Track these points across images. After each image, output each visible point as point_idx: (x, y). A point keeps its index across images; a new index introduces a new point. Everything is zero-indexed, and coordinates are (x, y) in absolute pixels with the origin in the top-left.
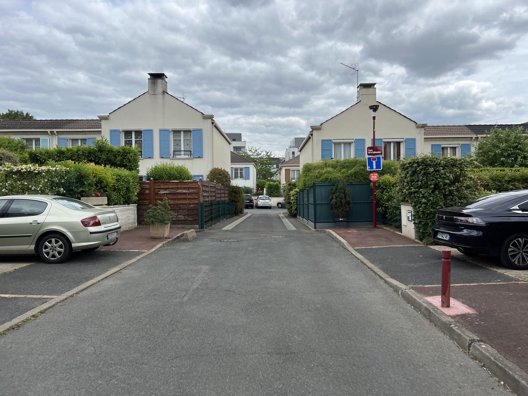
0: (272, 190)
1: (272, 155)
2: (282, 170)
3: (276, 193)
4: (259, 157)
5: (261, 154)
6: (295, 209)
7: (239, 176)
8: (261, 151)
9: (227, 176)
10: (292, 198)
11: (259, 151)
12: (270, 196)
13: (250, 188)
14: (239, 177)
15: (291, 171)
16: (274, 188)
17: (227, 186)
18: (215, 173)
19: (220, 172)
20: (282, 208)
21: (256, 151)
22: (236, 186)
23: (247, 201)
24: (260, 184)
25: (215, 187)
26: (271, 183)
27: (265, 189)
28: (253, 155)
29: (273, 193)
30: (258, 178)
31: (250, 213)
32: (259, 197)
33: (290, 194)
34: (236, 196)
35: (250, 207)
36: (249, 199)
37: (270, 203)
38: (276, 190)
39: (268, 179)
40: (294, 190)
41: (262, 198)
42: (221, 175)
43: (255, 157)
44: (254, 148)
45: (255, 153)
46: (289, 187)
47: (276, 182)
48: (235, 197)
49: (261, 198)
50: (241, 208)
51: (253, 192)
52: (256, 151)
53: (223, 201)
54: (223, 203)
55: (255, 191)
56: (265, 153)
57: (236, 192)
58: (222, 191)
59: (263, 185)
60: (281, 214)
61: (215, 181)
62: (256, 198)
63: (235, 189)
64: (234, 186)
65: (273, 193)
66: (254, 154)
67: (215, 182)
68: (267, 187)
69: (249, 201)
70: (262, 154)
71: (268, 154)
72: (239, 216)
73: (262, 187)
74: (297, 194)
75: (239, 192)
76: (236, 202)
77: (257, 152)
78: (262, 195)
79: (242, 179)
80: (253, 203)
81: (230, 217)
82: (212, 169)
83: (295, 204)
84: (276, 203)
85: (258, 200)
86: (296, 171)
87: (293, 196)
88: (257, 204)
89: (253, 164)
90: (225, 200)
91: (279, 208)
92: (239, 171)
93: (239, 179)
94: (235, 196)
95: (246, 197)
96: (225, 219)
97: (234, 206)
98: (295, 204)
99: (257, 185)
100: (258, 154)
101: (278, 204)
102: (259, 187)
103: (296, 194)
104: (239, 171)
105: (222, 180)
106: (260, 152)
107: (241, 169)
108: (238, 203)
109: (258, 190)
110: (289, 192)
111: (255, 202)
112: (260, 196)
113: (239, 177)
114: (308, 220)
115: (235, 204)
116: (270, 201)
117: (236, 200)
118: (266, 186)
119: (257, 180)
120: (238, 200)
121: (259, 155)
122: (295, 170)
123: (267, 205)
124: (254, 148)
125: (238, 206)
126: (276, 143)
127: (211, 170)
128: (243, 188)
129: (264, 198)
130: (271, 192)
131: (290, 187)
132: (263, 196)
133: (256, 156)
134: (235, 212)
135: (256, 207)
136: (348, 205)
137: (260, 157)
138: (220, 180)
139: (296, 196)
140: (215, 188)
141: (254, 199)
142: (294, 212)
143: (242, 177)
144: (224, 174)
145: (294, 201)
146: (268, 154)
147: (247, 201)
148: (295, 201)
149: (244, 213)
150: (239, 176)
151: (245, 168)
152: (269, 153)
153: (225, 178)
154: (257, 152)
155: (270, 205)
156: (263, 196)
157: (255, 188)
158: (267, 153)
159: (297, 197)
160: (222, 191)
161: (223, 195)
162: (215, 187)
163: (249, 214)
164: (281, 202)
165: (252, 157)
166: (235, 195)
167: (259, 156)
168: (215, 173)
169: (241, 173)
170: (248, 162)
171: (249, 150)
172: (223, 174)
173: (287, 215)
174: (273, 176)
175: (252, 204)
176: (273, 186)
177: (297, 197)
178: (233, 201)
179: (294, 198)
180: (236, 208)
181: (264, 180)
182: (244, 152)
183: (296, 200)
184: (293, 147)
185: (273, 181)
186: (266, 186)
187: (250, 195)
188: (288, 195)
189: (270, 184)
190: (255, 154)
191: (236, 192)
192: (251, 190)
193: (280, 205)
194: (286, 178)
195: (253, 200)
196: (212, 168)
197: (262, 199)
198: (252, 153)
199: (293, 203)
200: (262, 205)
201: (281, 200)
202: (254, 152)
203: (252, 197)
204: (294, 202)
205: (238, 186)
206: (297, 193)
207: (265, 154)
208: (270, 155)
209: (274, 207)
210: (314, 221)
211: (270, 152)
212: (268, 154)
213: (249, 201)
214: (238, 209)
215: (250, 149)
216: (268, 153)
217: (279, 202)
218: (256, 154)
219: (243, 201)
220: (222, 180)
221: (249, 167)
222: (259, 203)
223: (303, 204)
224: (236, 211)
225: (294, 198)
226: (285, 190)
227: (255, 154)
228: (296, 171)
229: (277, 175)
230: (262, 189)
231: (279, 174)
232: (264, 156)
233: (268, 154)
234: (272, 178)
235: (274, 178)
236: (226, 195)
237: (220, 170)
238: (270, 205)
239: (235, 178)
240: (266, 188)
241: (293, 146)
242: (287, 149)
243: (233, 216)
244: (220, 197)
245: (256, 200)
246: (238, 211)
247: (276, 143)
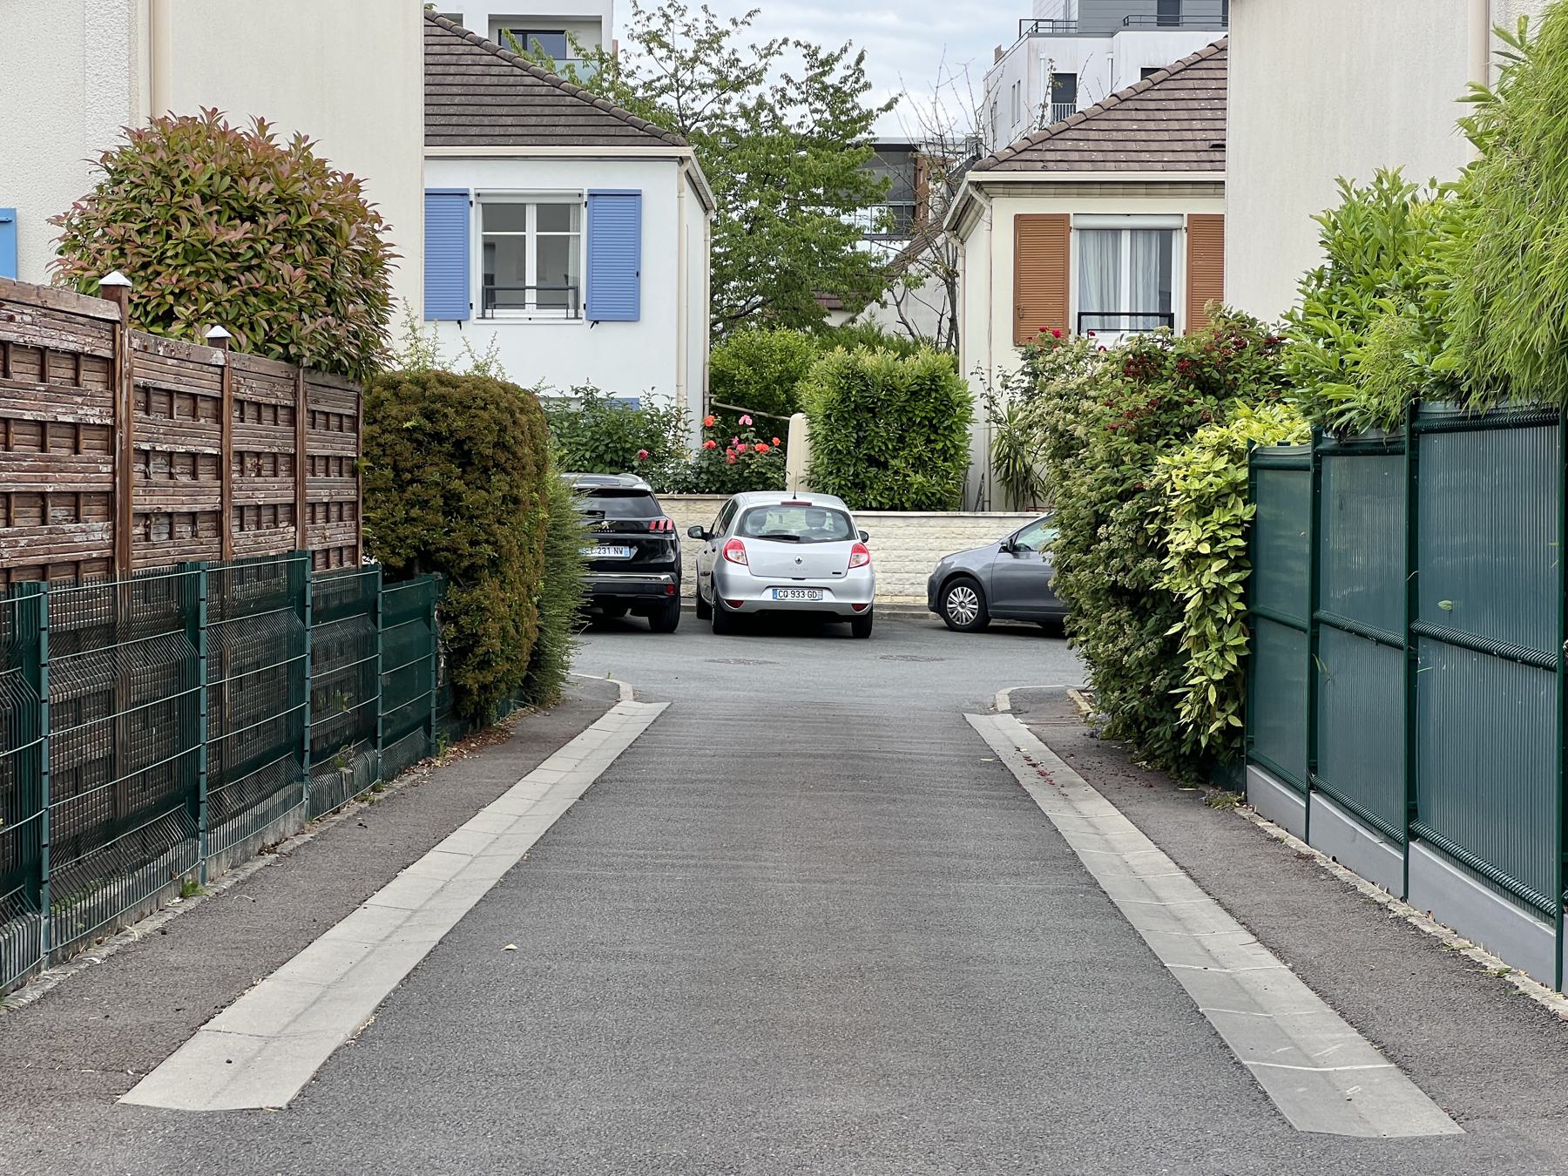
0: (883, 430)
1: (867, 86)
2: (982, 226)
3: (919, 464)
4: (742, 106)
5: (756, 77)
6: (1230, 677)
7: (531, 279)
8: (762, 45)
9: (333, 231)
10: (1184, 537)
11: (742, 45)
12: (857, 493)
13: (644, 404)
14: (531, 296)
15: (1074, 238)
16: (902, 410)
17: (336, 367)
18: (168, 181)
19: (239, 175)
20: (980, 626)
21: (713, 41)
22: (467, 378)
23: (611, 553)
24: (743, 372)
25: (109, 365)
26: (869, 361)
27: (798, 425)
28: (676, 85)
29: (884, 466)
30: (725, 320)
31: (639, 697)
32: (735, 506)
33: (1148, 484)
34: (472, 498)
35: (645, 620)
36: (638, 528)
37: (860, 575)
38: (920, 440)
39: (821, 328)
40: (1209, 435)
41: (773, 523)
42: (251, 214)
43: (697, 107)
44: (688, 19)
45: (699, 68)
46: (1141, 402)
47: (924, 353)
48: (452, 506)
49: (762, 522)
50: (527, 646)
51: (679, 456)
52: (713, 41)
53: (262, 568)
54: (264, 603)
55: (693, 444)
56: (804, 63)
57: (463, 455)
58: (246, 435)
59: (779, 381)
60: (993, 710)
61: (116, 278)
62: (706, 512)
63: (463, 407)
64: (445, 380)
65: (884, 466)
66: (686, 77)
67: (111, 292)
68: (828, 406)
69: (626, 553)
70: (772, 79)
71: (832, 80)
72: (504, 736)
73: (763, 401)
74: (1250, 492)
75: (500, 445)
76: (470, 576)
77: (725, 54)
78: (766, 484)
79: (561, 313)
80: (674, 568)
81: (378, 777)
82: (138, 136)
83: (1221, 623)
84: (925, 579)
85: (721, 543)
86: (1126, 238)
87: (1203, 507)
88: (717, 581)
89: (682, 160)
90: (297, 563)
91: (952, 627)
92: (531, 234)
93: (531, 310)
94: (451, 498)
95: (596, 504)
96: (297, 813)
97: (444, 618)
98: (1221, 623)
99: (718, 380)
100: (734, 73)
101: (945, 584)
102: (740, 399)
103: (1234, 487)
104: (531, 234)
105: (255, 279)
106: (748, 59)
107: (555, 214)
108: (488, 590)
109: (723, 428)
110: (1145, 463)
111: (692, 557)
112: (748, 500)
113: (531, 296)
114: (1312, 787)
115: (453, 592)
116: (858, 550)
117: (466, 548)
118: (815, 393)
119: (714, 336)
120: (488, 550)
121: (738, 86)
122: (1117, 231)
123: (828, 598)
124: (688, 19)
125: (493, 628)
126: (890, 19)
127: (114, 141)
128: (575, 407)
129: (797, 523)
130: (872, 461)
131: (1154, 390)
132: (786, 497)
133: (711, 95)
134: (459, 692)
135: (703, 610)
136: (1101, 541)
137: (751, 104)
138: (227, 280)
139: (1245, 512)
140: (111, 385)
141: (682, 532)
142: (1200, 725)
143: (557, 292)
144: (295, 201)
145: (1209, 580)
146: (828, 80)
147: (611, 553)
148: (1222, 573)
149: (568, 692)
150: (531, 279)
151: (592, 195)
152: (838, 67)
153: (302, 250)
154: (725, 54)
155: (857, 593)
156: (786, 497)
157: (696, 416)
158: (823, 64)
159: (1250, 531)
160: (246, 435)
161: (273, 490)
162: (109, 365)
163: (627, 704)
164: (974, 567)
165: (668, 100)
166: (458, 485)
167: (736, 97)
168: (168, 181)
169: (554, 253)
170: (633, 140)
171: (639, 30)
172: (285, 202)
173: (1075, 732)
174: (877, 297)
175: (662, 588)
176: (891, 390)
177: (1250, 531)
178: (426, 558)
179: (1214, 540)
180: (462, 651)
181: (785, 337)
182: (591, 50)
183: (1247, 559)
184: (1062, 29)
185: (873, 340)
186: (815, 393)
187: (641, 485)
188: (1124, 497)
189: (852, 375)
190: (703, 74)
191: (463, 455)
192: (654, 437)
193: (963, 603)
194: (1019, 313)
195: (673, 545)
196: (143, 124)
197: (764, 531)
198: (670, 66)
199: (1204, 612)
200: (767, 596)
201: (968, 544)
202: (689, 55)
203: (664, 506)
204: (1219, 593)
205: (492, 373)
206: (1253, 470)
207: (800, 75)
208: (855, 91)
209: (902, 617)
210: (660, 502)
211: (850, 58)
212: (828, 80)
213: (626, 553)
214: (485, 664)
215: (657, 24)
216: (828, 63)
217: (957, 564)
218: (710, 78)
219: (555, 557)
220: (255, 279)
221: (636, 195)
222: (733, 571)
223: (1413, 637)
224: (471, 680)
225: (1214, 540)
226: (1080, 431)
227: (703, 74)
228: (1126, 238)
229: (918, 283)
230: (770, 421)
231: (934, 281)
232: (792, 93)
233: (832, 80)
234: (862, 318)
235: (883, 317)
236: (324, 488)
237: (238, 144)
238: (857, 593)
239: (485, 306)
240: (819, 411)
241: (1060, 16)
242: (999, 54)
243: (430, 752)
244: (217, 516)
245: (706, 537)
246: (484, 688)
247: (890, 19)
